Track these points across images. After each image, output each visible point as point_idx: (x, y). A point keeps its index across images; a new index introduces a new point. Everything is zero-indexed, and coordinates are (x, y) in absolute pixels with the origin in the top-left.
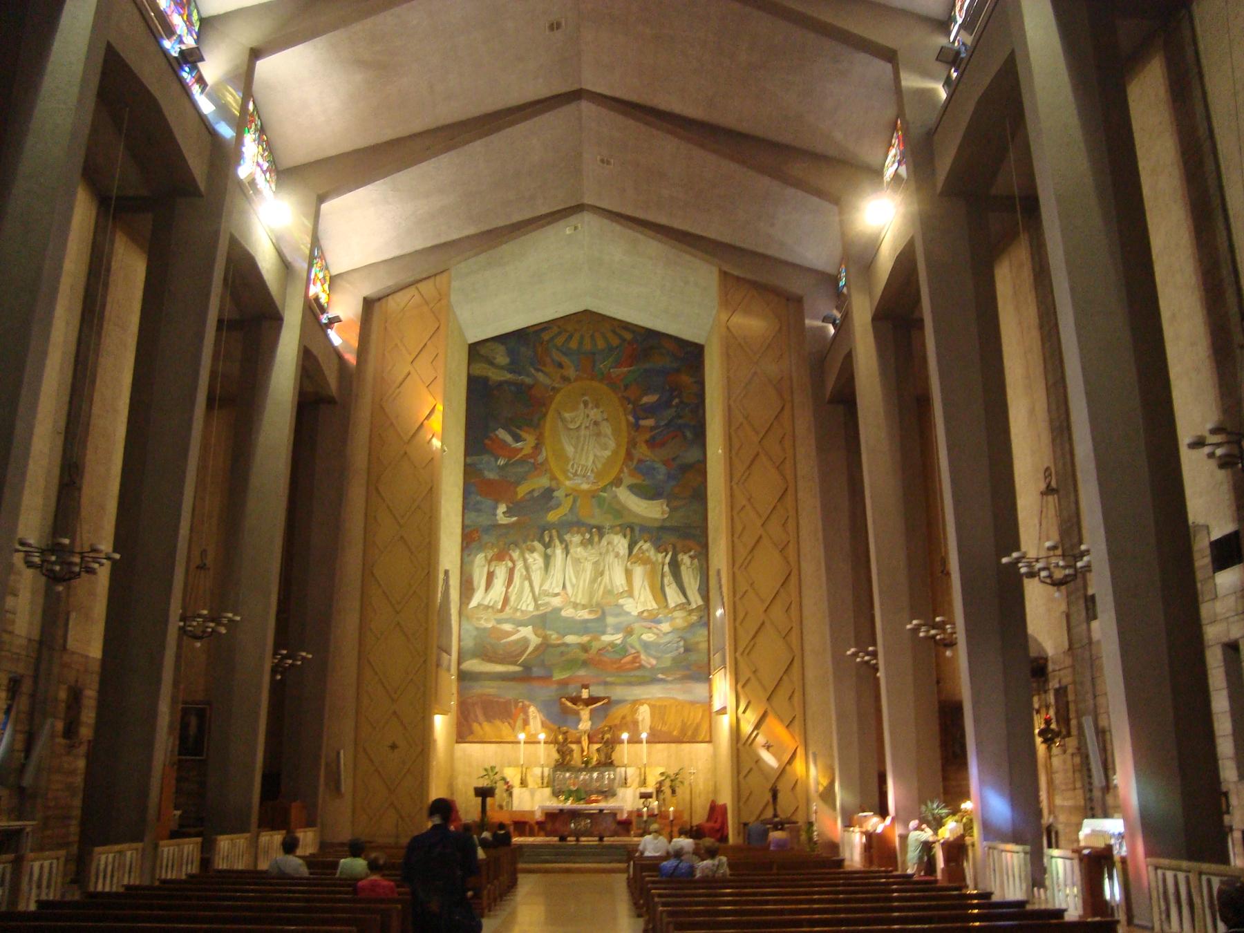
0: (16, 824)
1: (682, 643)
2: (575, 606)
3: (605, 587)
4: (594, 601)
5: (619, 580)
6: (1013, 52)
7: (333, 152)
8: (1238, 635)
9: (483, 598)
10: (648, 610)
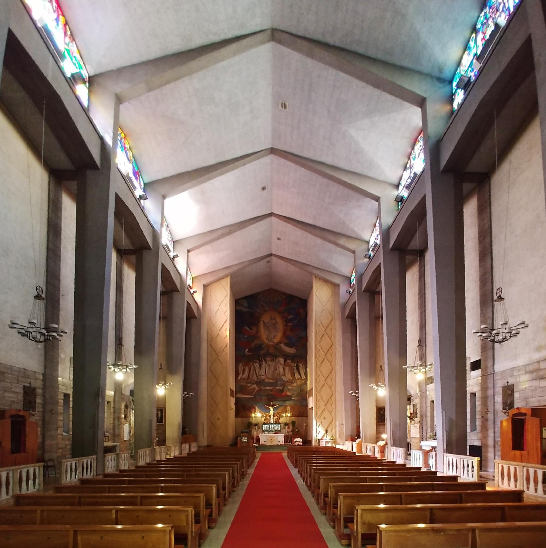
0: (115, 444)
1: (299, 389)
2: (269, 378)
3: (277, 373)
4: (274, 377)
5: (281, 371)
6: (425, 195)
7: (191, 235)
8: (476, 390)
9: (242, 376)
10: (290, 380)
